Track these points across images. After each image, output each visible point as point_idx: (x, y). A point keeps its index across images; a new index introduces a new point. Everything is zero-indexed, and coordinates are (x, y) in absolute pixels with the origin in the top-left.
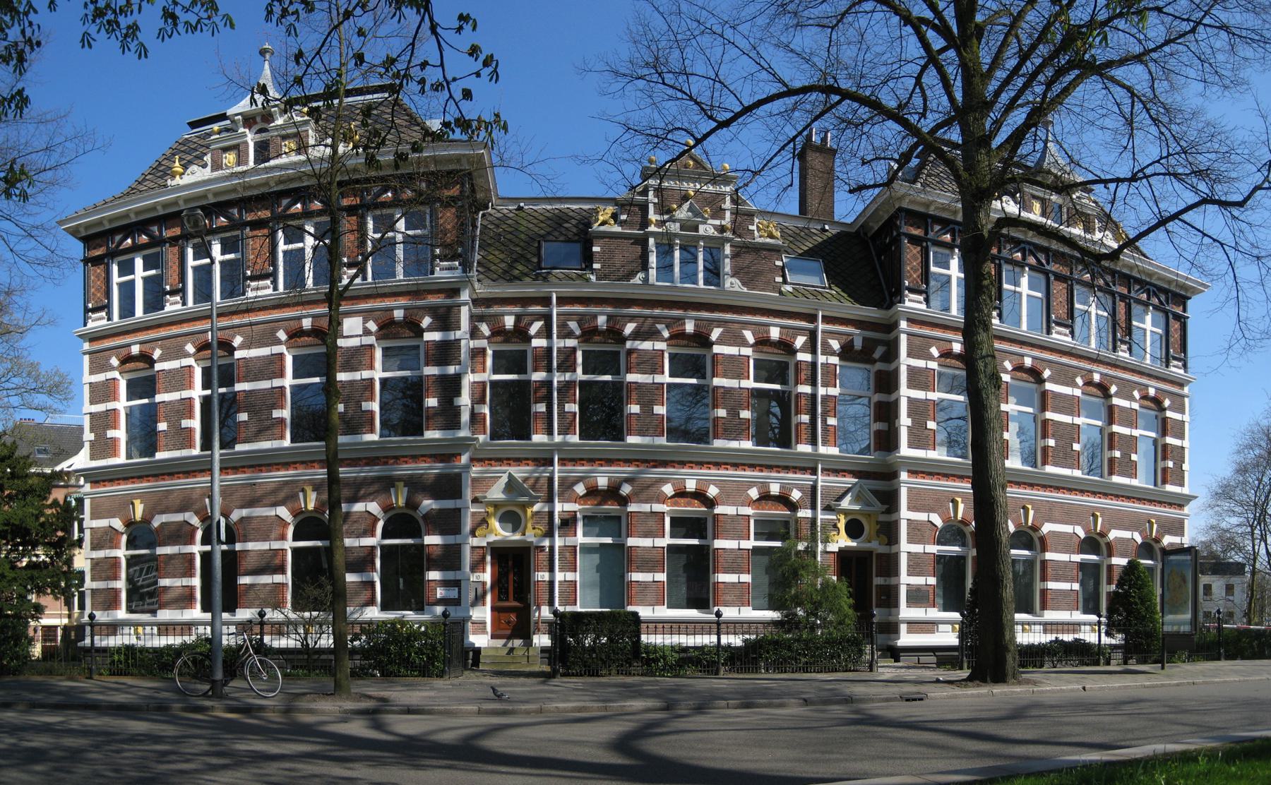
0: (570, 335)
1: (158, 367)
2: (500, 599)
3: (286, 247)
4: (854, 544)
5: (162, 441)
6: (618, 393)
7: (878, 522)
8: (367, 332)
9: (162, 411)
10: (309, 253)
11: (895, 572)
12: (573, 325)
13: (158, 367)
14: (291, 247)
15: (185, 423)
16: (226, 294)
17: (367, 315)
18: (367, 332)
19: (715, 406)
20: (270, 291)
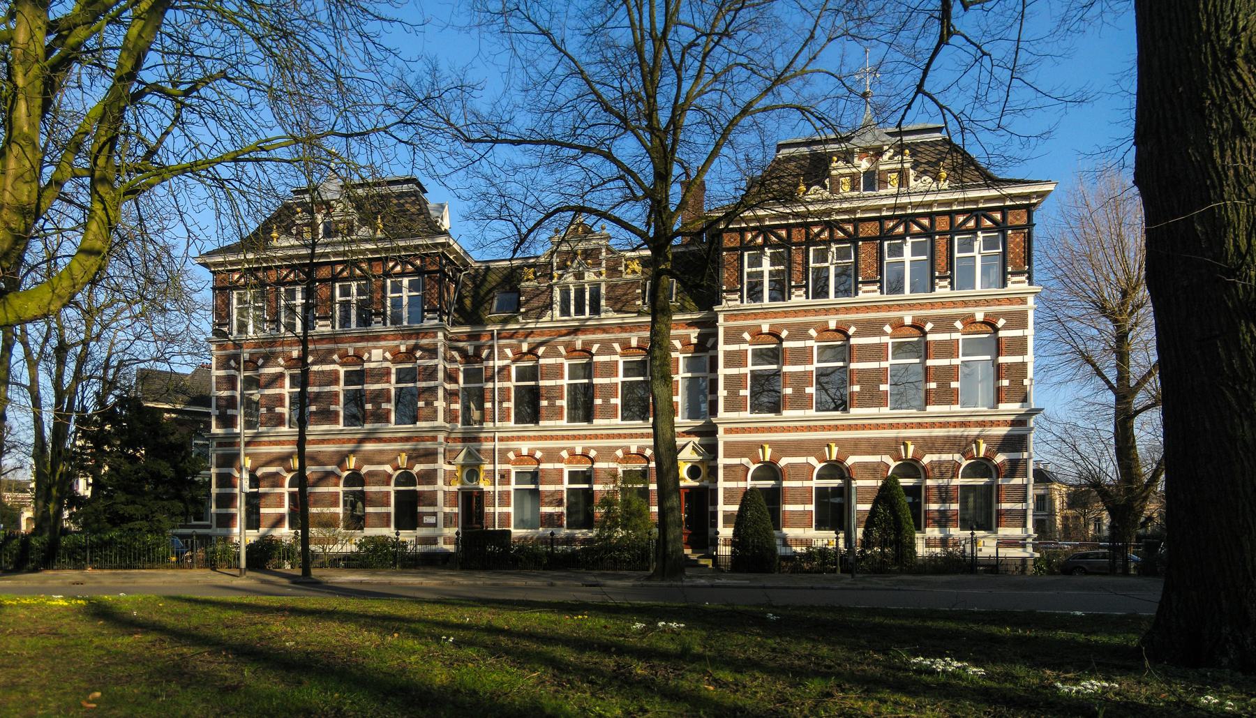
0: (506, 357)
1: (596, 359)
2: (841, 506)
3: (749, 270)
4: (697, 484)
5: (597, 412)
6: (589, 391)
7: (709, 467)
8: (385, 359)
9: (597, 392)
10: (405, 301)
11: (715, 503)
12: (508, 352)
13: (786, 344)
14: (818, 265)
15: (558, 403)
16: (577, 313)
17: (385, 349)
18: (385, 359)
19: (851, 383)
20: (329, 328)
